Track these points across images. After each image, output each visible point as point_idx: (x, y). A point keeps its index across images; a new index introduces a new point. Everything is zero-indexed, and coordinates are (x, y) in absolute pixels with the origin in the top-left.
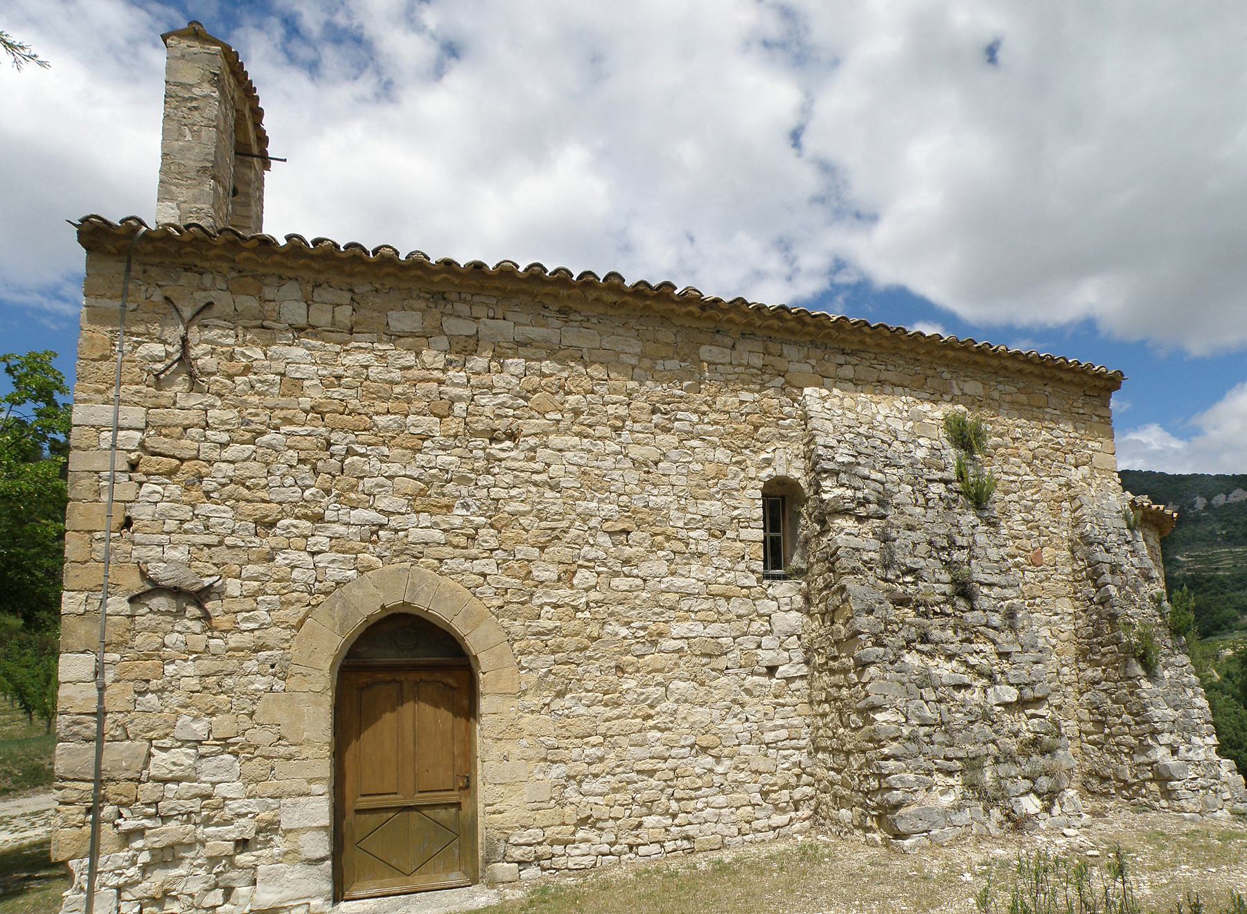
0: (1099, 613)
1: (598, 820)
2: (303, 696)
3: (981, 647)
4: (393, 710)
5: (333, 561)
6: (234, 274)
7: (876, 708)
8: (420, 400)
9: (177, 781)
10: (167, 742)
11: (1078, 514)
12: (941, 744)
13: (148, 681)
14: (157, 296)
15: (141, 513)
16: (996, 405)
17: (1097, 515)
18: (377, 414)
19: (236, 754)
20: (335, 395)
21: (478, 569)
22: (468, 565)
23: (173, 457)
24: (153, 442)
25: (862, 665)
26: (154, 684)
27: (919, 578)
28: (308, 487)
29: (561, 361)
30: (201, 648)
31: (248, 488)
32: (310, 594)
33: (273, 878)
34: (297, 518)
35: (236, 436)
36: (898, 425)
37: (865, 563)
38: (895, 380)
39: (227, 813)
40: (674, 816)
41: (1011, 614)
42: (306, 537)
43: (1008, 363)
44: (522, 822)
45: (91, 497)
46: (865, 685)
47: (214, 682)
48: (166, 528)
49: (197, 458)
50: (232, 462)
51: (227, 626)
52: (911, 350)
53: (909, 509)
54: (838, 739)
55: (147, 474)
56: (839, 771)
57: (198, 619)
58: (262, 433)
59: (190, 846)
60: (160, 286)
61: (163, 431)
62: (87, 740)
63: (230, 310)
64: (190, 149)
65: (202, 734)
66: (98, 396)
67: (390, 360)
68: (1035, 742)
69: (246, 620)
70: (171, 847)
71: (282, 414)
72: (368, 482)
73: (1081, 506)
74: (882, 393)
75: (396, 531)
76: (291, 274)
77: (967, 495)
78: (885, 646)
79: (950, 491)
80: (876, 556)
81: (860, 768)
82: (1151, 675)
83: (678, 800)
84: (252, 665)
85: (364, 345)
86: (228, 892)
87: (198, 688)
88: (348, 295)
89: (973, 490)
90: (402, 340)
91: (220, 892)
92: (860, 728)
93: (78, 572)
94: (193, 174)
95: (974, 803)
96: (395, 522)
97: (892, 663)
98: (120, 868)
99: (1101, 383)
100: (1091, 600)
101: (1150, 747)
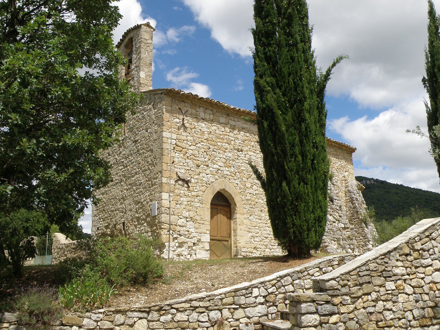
1: (258, 248)
2: (206, 209)
9: (183, 227)
11: (347, 184)
14: (177, 108)
15: (176, 160)
17: (351, 185)
21: (236, 182)
22: (234, 181)
24: (178, 143)
26: (179, 202)
29: (250, 134)
33: (200, 253)
39: (192, 236)
40: (271, 250)
41: (340, 207)
43: (333, 144)
47: (190, 203)
51: (192, 190)
55: (177, 151)
58: (197, 144)
64: (147, 57)
68: (349, 237)
69: (195, 189)
70: (182, 243)
71: (201, 139)
72: (217, 158)
82: (367, 228)
83: (272, 246)
84: (196, 200)
86: (191, 255)
91: (190, 255)
94: (148, 65)
96: (221, 169)
99: (351, 150)
100: (351, 207)
101: (368, 245)
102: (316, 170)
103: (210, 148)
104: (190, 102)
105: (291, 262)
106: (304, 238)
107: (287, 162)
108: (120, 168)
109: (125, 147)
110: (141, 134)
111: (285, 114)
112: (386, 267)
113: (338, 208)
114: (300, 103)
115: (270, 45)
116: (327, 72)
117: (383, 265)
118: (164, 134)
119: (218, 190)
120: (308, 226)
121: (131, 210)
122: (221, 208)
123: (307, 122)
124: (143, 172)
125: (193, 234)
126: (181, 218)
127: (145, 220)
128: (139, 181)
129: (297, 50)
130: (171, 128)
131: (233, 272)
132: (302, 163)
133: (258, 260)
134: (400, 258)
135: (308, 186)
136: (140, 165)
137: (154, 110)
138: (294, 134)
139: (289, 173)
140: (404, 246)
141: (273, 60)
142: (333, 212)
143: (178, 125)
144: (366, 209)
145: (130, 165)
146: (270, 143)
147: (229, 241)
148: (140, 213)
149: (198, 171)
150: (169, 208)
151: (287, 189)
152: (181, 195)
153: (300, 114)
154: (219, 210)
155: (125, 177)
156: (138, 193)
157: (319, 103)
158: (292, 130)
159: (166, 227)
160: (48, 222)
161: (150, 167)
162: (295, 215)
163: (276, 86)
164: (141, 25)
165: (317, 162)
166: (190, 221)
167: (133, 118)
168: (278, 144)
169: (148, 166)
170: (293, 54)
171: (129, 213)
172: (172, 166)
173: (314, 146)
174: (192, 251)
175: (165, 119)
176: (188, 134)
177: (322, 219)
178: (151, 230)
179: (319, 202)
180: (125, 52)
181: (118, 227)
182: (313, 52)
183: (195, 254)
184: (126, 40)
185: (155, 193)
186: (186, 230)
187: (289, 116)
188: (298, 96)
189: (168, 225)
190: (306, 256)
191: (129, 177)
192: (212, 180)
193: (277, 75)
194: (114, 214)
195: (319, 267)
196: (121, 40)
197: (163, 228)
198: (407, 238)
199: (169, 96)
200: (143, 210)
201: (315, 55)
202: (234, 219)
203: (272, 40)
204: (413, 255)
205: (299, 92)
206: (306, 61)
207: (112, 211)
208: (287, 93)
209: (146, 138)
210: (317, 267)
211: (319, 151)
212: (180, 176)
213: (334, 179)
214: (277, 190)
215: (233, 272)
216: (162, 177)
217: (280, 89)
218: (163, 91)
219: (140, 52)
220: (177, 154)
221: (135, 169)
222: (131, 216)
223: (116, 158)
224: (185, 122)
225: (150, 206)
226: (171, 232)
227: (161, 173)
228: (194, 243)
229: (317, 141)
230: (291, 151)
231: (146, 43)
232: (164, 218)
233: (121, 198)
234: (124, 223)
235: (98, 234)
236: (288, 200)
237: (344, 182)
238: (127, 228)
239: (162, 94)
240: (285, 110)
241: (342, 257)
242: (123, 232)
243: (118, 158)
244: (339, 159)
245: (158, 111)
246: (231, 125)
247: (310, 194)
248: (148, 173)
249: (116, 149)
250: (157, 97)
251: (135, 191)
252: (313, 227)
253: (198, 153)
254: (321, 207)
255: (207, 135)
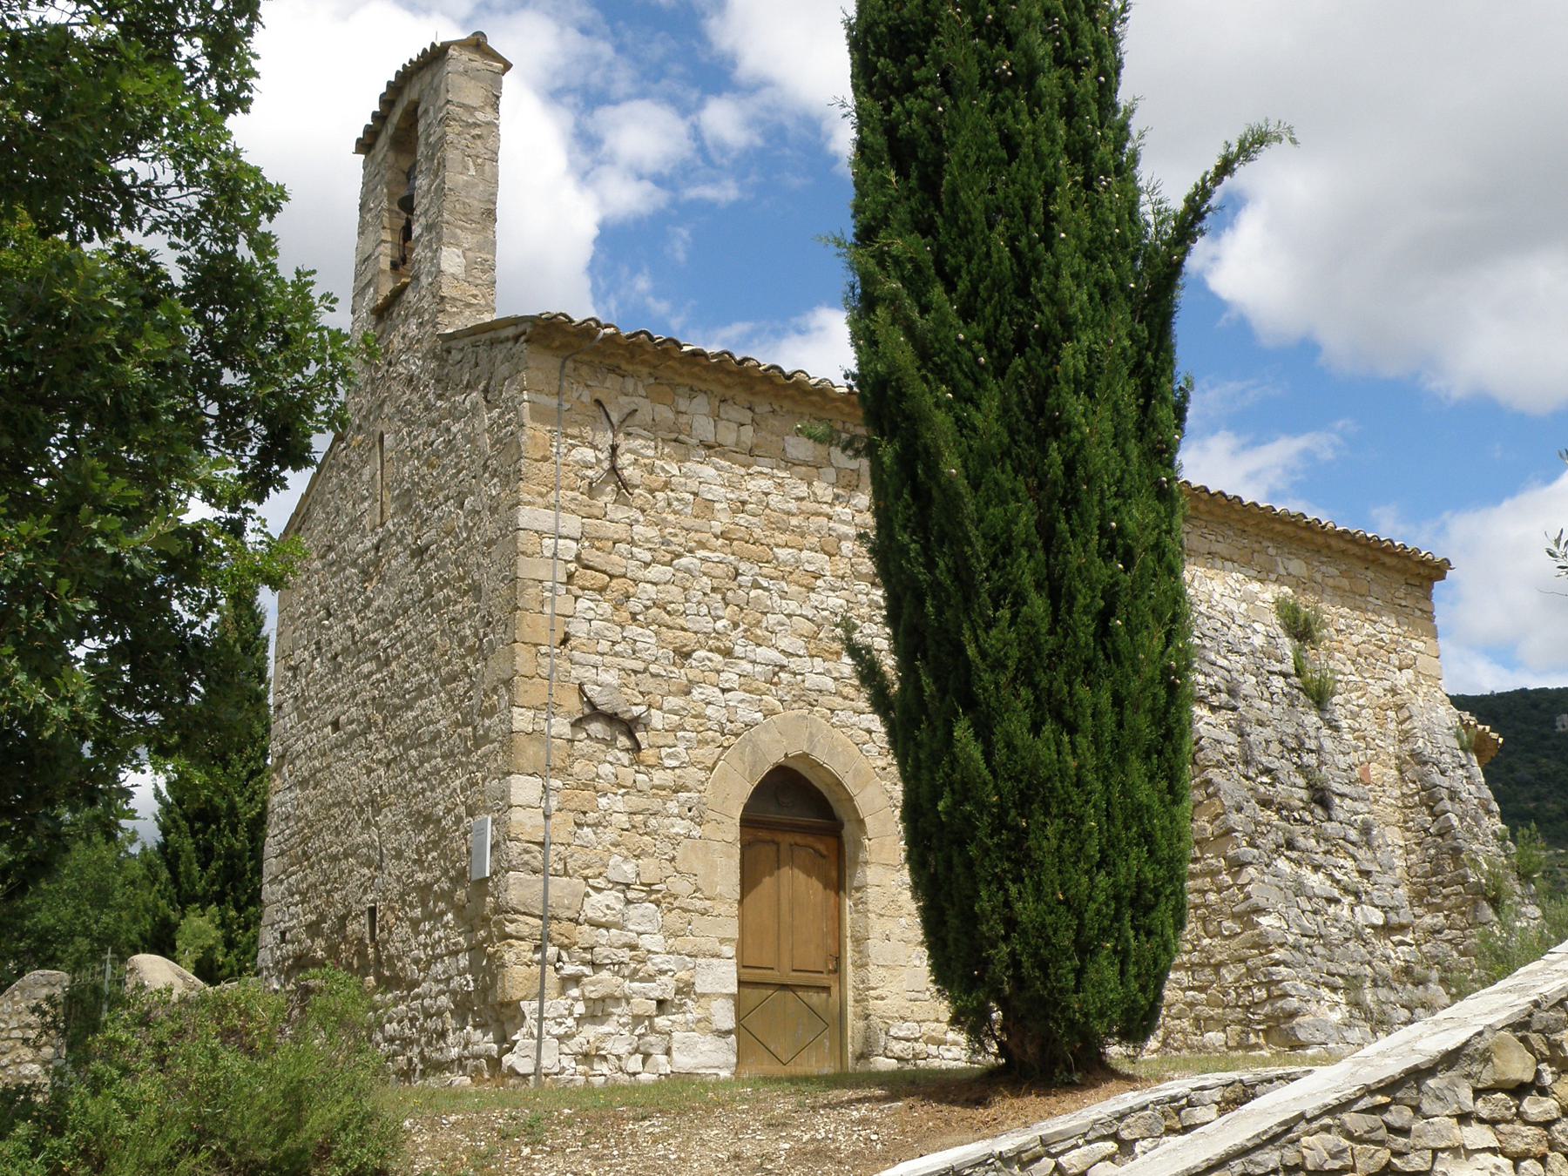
0: (1437, 847)
2: (717, 846)
3: (1342, 862)
4: (771, 874)
5: (742, 701)
6: (652, 381)
7: (1259, 911)
8: (812, 534)
9: (607, 926)
10: (600, 882)
11: (1406, 726)
12: (1323, 956)
13: (584, 813)
14: (587, 398)
15: (579, 629)
16: (1320, 589)
18: (778, 546)
19: (657, 903)
20: (742, 522)
21: (865, 725)
22: (855, 719)
23: (604, 572)
25: (1238, 865)
26: (592, 817)
27: (1275, 780)
28: (720, 618)
30: (629, 783)
31: (668, 613)
32: (723, 734)
33: (688, 1047)
34: (711, 650)
35: (659, 558)
36: (1232, 606)
37: (1227, 756)
38: (1225, 553)
39: (650, 968)
41: (1366, 830)
42: (718, 672)
43: (1333, 542)
44: (902, 1013)
45: (538, 608)
46: (1244, 886)
47: (642, 818)
48: (600, 648)
49: (624, 576)
50: (655, 584)
51: (652, 761)
52: (1241, 521)
53: (1257, 703)
54: (1201, 951)
55: (583, 588)
56: (1202, 989)
57: (627, 750)
58: (679, 556)
59: (617, 1000)
60: (588, 386)
61: (597, 544)
62: (535, 872)
63: (649, 419)
65: (631, 877)
66: (539, 500)
67: (787, 488)
68: (1407, 971)
69: (669, 756)
70: (603, 999)
71: (697, 536)
72: (771, 619)
73: (1410, 717)
74: (1213, 567)
75: (795, 674)
76: (703, 387)
77: (1304, 690)
78: (1257, 847)
79: (1290, 685)
80: (1235, 750)
81: (1237, 980)
84: (673, 807)
85: (765, 470)
86: (647, 1056)
87: (627, 826)
88: (750, 414)
89: (1313, 687)
90: (797, 469)
91: (640, 1057)
92: (1238, 934)
93: (527, 687)
94: (476, 217)
95: (1361, 1023)
96: (794, 663)
97: (1267, 866)
98: (561, 1016)
99: (1423, 571)
100: (1426, 830)
102: (1119, 663)
103: (737, 574)
104: (645, 370)
105: (1002, 1106)
106: (1061, 991)
107: (974, 629)
108: (366, 668)
109: (382, 579)
110: (440, 518)
111: (970, 400)
112: (1397, 1154)
113: (1353, 835)
114: (1045, 349)
115: (910, 86)
116: (1190, 200)
117: (1381, 1143)
118: (525, 516)
119: (778, 757)
120: (1078, 933)
121: (399, 855)
122: (798, 838)
123: (1075, 435)
124: (443, 684)
125: (657, 959)
126: (598, 890)
127: (447, 896)
128: (428, 723)
129: (1035, 101)
130: (556, 487)
131: (723, 1156)
132: (1052, 632)
133: (861, 1093)
134: (1483, 1108)
135: (1079, 738)
136: (436, 655)
137: (490, 410)
138: (1014, 492)
139: (986, 676)
140: (1501, 1045)
141: (921, 155)
142: (1327, 852)
143: (590, 473)
144: (1502, 839)
145: (398, 656)
146: (904, 538)
147: (835, 991)
148: (429, 869)
149: (681, 675)
150: (542, 844)
151: (978, 755)
152: (601, 784)
153: (1041, 394)
154: (784, 847)
155: (379, 709)
156: (425, 779)
157: (1148, 348)
158: (1003, 476)
159: (525, 931)
160: (171, 903)
161: (469, 661)
162: (1018, 879)
163: (933, 271)
164: (446, 47)
165: (1127, 622)
166: (641, 901)
167: (412, 451)
168: (941, 543)
169: (463, 657)
170: (1010, 121)
171: (391, 865)
172: (558, 656)
173: (1112, 547)
174: (651, 1038)
175: (529, 450)
176: (638, 515)
177: (1157, 896)
178: (469, 941)
179: (1138, 812)
180: (390, 167)
181: (353, 927)
182: (1129, 112)
183: (668, 1052)
184: (396, 116)
185: (484, 779)
186: (624, 940)
187: (987, 416)
188: (1032, 318)
189: (539, 922)
190: (1076, 1078)
191: (397, 708)
192: (747, 714)
193: (939, 221)
194: (342, 872)
195: (1115, 1137)
196: (374, 115)
197: (511, 937)
198: (1523, 1002)
199: (548, 347)
200: (443, 856)
201: (1135, 125)
202: (858, 889)
203: (923, 63)
204: (1557, 1088)
205: (1041, 296)
206: (1081, 153)
207: (334, 859)
208: (979, 304)
209: (457, 537)
210: (1104, 1138)
211: (1135, 571)
212: (597, 700)
213: (1335, 699)
214: (936, 760)
215: (723, 1156)
216: (512, 704)
217: (950, 287)
218: (520, 329)
219: (442, 164)
220: (583, 604)
221: (417, 674)
222: (399, 879)
223: (351, 628)
224: (624, 459)
225: (465, 834)
226: (552, 951)
227: (509, 690)
228: (661, 1003)
229: (1131, 526)
230: (995, 576)
231: (469, 125)
232: (519, 888)
233: (366, 803)
234: (372, 911)
235: (285, 959)
236: (982, 806)
237: (1391, 714)
238: (385, 934)
239: (516, 339)
240: (969, 384)
241: (1238, 1088)
242: (370, 950)
243: (359, 627)
244: (1365, 611)
245: (501, 415)
246: (838, 470)
247: (1090, 777)
248: (461, 691)
249: (351, 590)
250: (499, 353)
251: (414, 769)
252: (1105, 933)
253: (681, 598)
254: (1147, 837)
255: (725, 518)
